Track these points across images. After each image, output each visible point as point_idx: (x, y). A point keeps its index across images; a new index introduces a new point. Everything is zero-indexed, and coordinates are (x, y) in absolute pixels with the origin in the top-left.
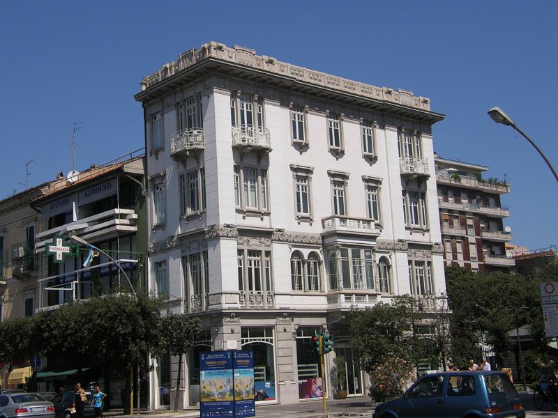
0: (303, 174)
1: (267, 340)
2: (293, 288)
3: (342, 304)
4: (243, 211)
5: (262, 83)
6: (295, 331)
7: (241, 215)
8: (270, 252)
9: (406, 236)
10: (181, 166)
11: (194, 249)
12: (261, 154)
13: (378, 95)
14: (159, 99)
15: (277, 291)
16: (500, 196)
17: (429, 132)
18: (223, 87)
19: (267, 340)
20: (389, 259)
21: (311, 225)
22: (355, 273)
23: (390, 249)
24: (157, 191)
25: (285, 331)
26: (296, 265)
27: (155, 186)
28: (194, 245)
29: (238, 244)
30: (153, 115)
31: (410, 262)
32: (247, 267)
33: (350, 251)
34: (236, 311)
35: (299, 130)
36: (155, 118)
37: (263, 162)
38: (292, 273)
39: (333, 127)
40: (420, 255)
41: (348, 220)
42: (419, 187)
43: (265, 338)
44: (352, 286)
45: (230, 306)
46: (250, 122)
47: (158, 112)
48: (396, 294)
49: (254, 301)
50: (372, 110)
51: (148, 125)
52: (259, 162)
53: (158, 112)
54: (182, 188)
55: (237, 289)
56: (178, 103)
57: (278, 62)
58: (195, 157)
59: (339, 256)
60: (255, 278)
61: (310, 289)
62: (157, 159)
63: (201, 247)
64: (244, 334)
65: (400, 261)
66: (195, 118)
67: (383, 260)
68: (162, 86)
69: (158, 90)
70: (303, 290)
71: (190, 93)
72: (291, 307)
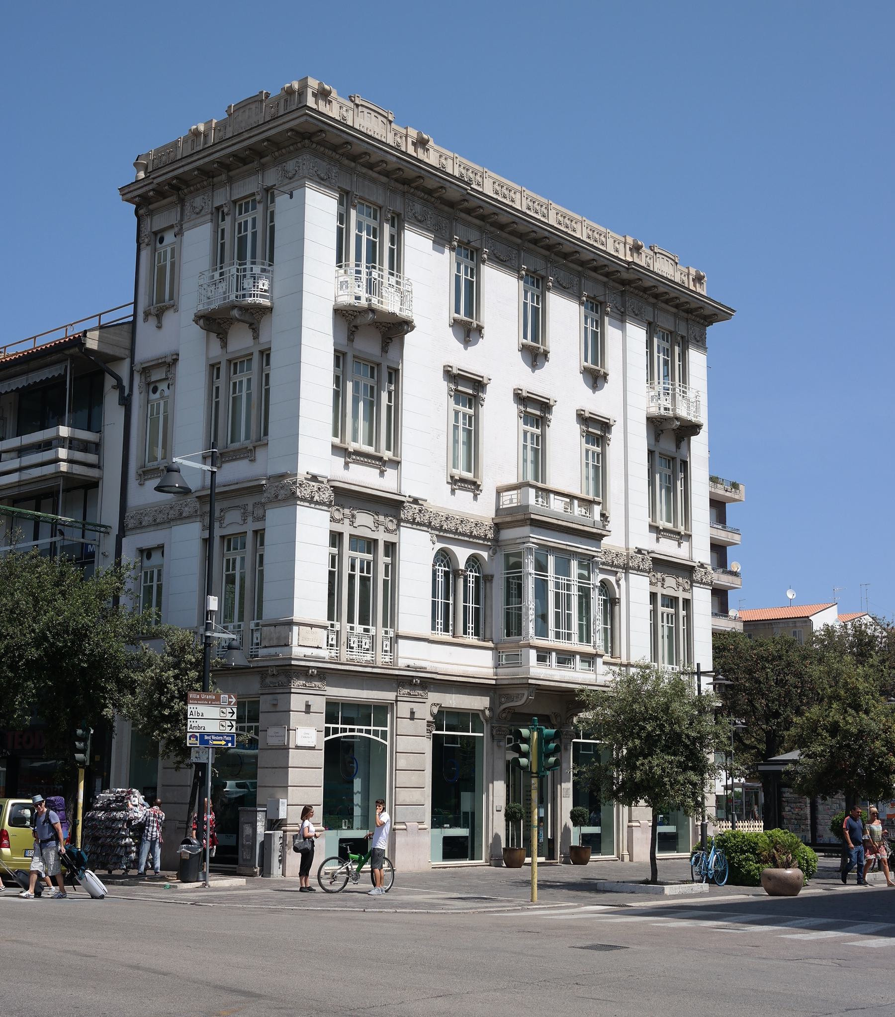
0: (468, 389)
1: (376, 733)
2: (434, 628)
3: (531, 670)
4: (346, 449)
6: (431, 719)
7: (341, 461)
9: (646, 541)
10: (216, 343)
11: (232, 522)
14: (173, 198)
16: (728, 506)
17: (701, 343)
18: (324, 182)
19: (376, 733)
20: (616, 586)
21: (475, 497)
22: (557, 606)
24: (153, 397)
25: (412, 717)
27: (149, 384)
28: (234, 516)
29: (333, 519)
31: (653, 596)
32: (346, 571)
33: (551, 560)
34: (320, 665)
35: (468, 295)
36: (161, 241)
37: (392, 352)
39: (529, 301)
40: (671, 586)
41: (552, 496)
44: (552, 634)
45: (308, 652)
46: (371, 259)
49: (355, 645)
50: (605, 279)
51: (145, 254)
52: (384, 349)
54: (213, 392)
55: (323, 619)
56: (218, 209)
57: (436, 147)
58: (251, 325)
59: (530, 567)
60: (363, 595)
61: (465, 633)
62: (159, 327)
63: (250, 519)
64: (331, 718)
65: (636, 591)
66: (261, 244)
67: (605, 586)
68: (186, 168)
69: (176, 177)
70: (451, 633)
71: (249, 186)
72: (429, 666)
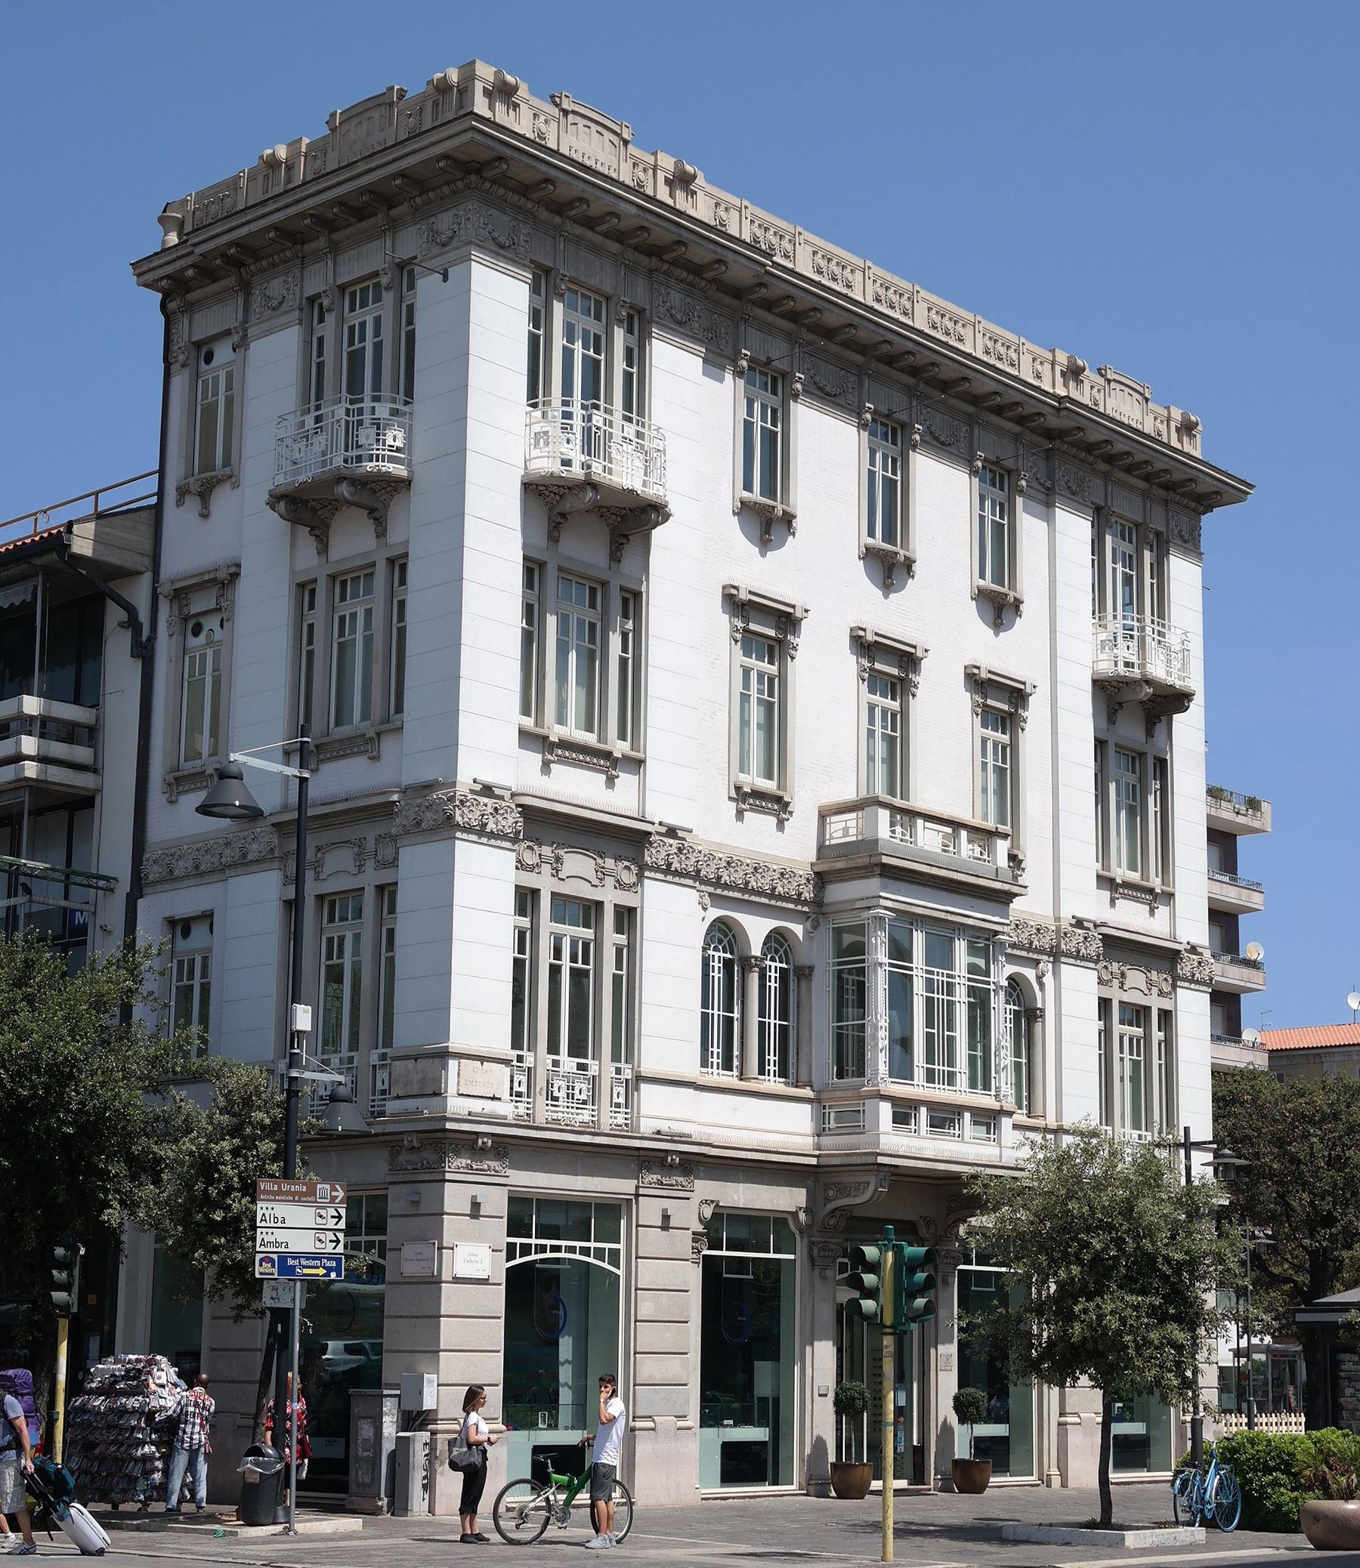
0: (766, 628)
1: (599, 1254)
2: (704, 1063)
3: (883, 1139)
4: (545, 738)
5: (650, 255)
6: (700, 1228)
7: (535, 759)
8: (632, 911)
10: (307, 545)
12: (632, 520)
13: (1039, 377)
14: (230, 282)
15: (647, 1067)
17: (1191, 545)
18: (504, 251)
19: (599, 1254)
20: (1036, 987)
21: (781, 825)
22: (929, 1023)
23: (1040, 951)
24: (193, 642)
26: (717, 975)
27: (186, 619)
28: (340, 860)
29: (521, 866)
30: (198, 345)
31: (1104, 1004)
32: (545, 959)
33: (919, 939)
35: (768, 458)
36: (209, 358)
38: (705, 1003)
40: (1137, 985)
41: (920, 822)
42: (1150, 733)
43: (592, 1245)
44: (919, 1074)
45: (477, 1106)
46: (592, 390)
47: (227, 333)
48: (1051, 1121)
49: (562, 1095)
50: (1017, 428)
51: (179, 382)
53: (227, 333)
54: (303, 634)
55: (502, 1044)
56: (311, 300)
57: (709, 188)
58: (372, 511)
59: (880, 953)
60: (575, 1002)
61: (762, 1071)
62: (205, 515)
63: (370, 865)
64: (517, 1226)
65: (1074, 995)
68: (254, 227)
69: (235, 243)
70: (735, 1073)
71: (368, 259)
72: (695, 1131)
